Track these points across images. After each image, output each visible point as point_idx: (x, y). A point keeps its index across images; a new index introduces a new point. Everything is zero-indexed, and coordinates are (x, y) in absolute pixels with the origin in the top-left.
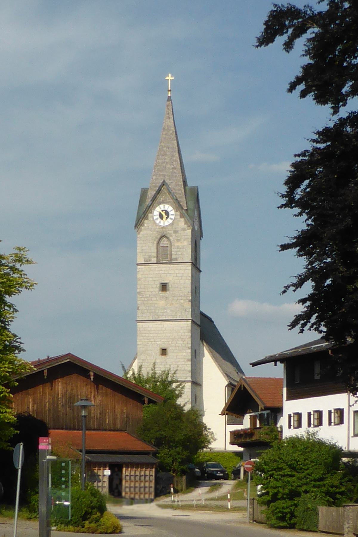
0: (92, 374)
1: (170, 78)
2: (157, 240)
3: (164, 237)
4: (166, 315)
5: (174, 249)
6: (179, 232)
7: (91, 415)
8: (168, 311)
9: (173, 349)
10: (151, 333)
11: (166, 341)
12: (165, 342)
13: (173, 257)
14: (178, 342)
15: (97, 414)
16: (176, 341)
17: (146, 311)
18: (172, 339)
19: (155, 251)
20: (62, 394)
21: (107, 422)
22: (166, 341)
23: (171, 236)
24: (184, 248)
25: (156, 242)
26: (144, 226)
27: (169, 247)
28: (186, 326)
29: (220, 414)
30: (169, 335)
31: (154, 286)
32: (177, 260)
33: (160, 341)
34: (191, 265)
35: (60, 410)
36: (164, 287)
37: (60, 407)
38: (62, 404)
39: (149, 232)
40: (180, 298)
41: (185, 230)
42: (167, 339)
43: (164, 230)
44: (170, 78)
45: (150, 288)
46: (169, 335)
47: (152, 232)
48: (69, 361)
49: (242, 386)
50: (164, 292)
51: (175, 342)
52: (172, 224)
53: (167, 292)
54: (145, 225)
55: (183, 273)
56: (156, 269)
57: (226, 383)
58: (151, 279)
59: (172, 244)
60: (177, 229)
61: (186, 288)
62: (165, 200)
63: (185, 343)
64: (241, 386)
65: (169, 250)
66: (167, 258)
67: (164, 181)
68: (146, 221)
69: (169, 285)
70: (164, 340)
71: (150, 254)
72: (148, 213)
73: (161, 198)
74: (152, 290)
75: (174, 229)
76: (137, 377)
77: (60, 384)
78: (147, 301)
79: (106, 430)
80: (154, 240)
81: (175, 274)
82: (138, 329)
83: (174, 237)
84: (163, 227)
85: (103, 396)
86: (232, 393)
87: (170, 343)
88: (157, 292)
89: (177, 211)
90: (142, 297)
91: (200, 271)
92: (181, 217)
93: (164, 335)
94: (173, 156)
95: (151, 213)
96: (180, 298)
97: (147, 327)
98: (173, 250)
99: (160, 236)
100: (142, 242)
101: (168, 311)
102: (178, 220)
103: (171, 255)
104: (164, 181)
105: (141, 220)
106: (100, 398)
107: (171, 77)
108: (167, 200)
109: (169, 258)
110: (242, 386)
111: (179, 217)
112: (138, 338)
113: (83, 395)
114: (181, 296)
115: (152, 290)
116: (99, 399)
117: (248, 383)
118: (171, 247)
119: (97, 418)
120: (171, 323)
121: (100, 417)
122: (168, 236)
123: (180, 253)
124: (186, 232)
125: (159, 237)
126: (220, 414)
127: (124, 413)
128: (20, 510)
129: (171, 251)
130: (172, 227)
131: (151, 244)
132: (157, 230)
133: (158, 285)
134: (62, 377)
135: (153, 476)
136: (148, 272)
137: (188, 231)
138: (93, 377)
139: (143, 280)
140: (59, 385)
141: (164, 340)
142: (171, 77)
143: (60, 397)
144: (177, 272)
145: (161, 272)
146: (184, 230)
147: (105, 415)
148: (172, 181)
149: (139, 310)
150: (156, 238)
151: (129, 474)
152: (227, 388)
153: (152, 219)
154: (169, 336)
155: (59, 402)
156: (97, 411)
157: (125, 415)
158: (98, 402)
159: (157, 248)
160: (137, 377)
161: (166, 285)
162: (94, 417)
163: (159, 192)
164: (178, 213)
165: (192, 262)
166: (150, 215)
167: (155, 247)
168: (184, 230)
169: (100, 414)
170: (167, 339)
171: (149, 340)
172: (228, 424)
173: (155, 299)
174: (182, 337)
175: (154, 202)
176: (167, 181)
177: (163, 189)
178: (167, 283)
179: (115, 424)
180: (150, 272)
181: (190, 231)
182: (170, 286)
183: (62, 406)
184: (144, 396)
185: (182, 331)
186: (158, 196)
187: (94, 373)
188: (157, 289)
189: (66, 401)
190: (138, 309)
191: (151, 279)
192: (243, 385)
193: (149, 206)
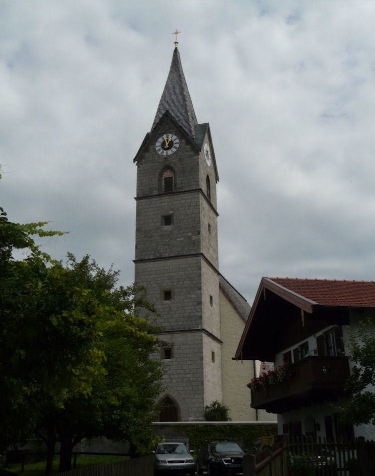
9: (179, 290)
13: (178, 186)
29: (233, 359)
32: (182, 189)
36: (168, 220)
64: (263, 292)
74: (153, 225)
76: (125, 280)
83: (179, 166)
84: (166, 158)
86: (271, 279)
91: (217, 215)
117: (221, 371)
120: (177, 260)
123: (186, 182)
126: (233, 359)
128: (231, 420)
135: (256, 422)
159: (160, 180)
160: (125, 280)
164: (184, 141)
166: (151, 147)
171: (148, 283)
174: (190, 276)
178: (171, 216)
180: (151, 206)
185: (190, 269)
191: (152, 213)
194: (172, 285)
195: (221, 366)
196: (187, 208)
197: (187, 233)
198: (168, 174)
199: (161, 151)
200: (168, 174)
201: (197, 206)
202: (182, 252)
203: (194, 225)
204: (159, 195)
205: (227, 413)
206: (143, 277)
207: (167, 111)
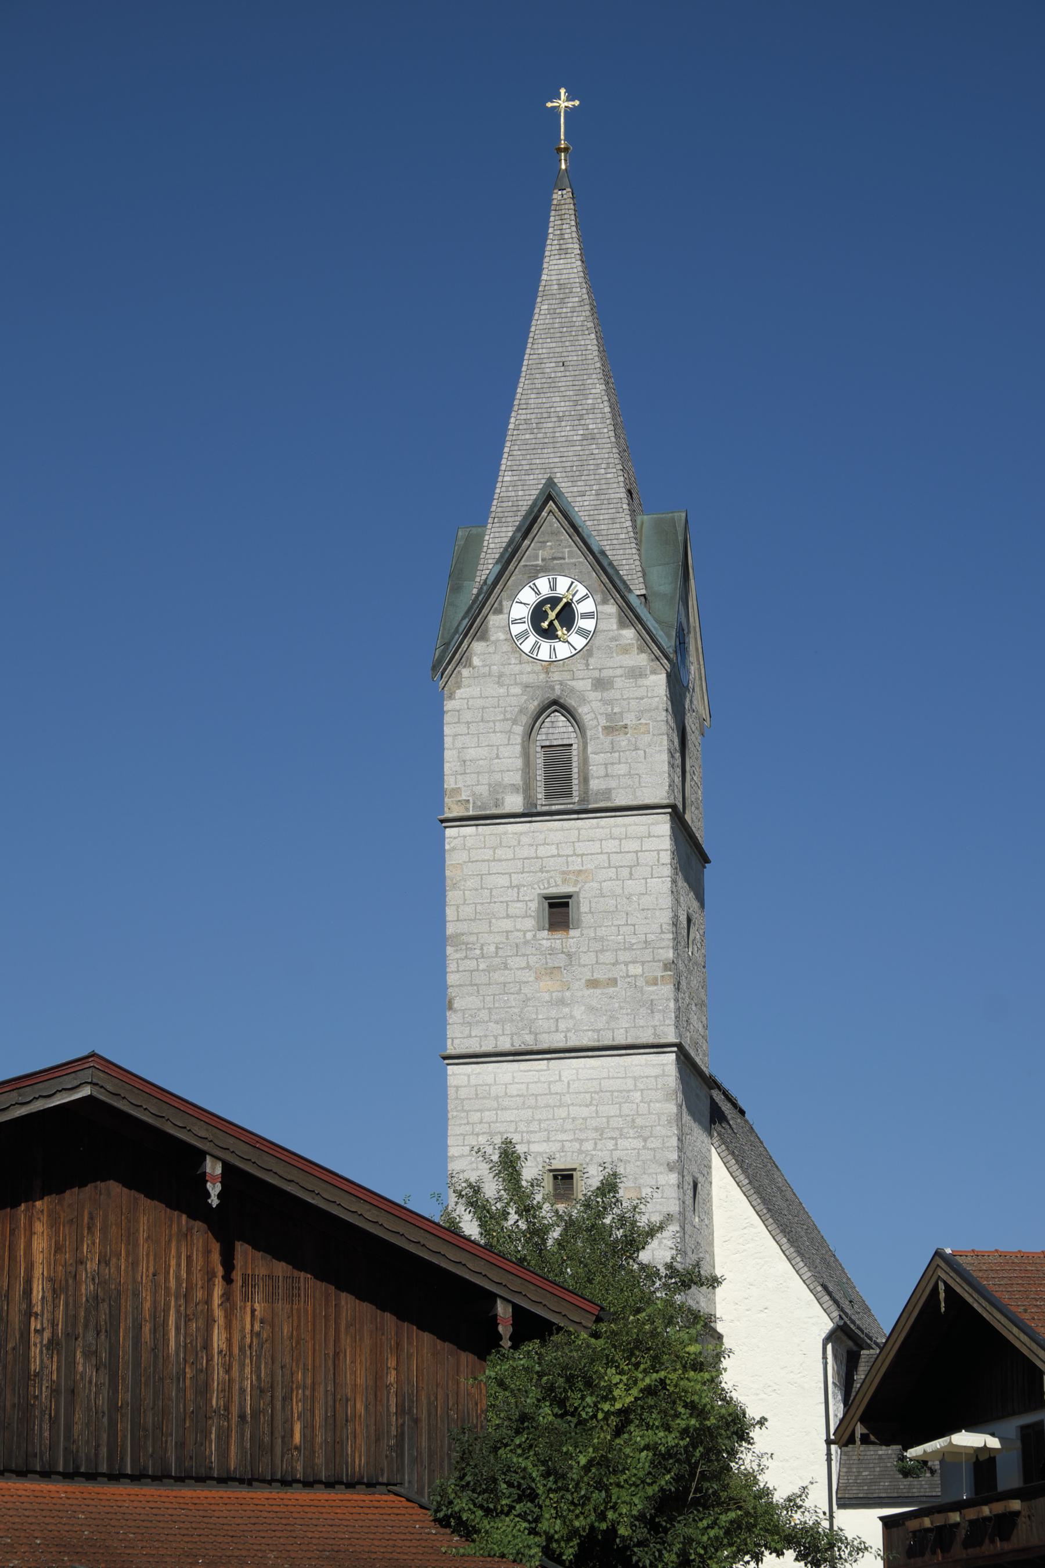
0: (213, 1168)
1: (563, 102)
2: (524, 719)
3: (554, 708)
4: (568, 1030)
5: (596, 753)
6: (619, 683)
7: (208, 1401)
8: (578, 1012)
10: (505, 1109)
11: (571, 1141)
12: (568, 1144)
13: (594, 784)
14: (622, 1143)
15: (242, 1391)
16: (612, 1138)
17: (483, 1015)
18: (596, 1129)
19: (519, 763)
20: (50, 1279)
21: (297, 1438)
22: (571, 1141)
23: (584, 700)
24: (637, 749)
25: (519, 729)
26: (469, 664)
27: (575, 747)
28: (657, 1071)
30: (585, 1112)
31: (517, 908)
33: (548, 1140)
34: (668, 817)
35: (35, 1366)
37: (35, 1351)
38: (47, 1335)
39: (493, 690)
40: (627, 953)
41: (642, 675)
42: (574, 1131)
43: (556, 677)
44: (563, 102)
45: (497, 919)
46: (585, 1112)
47: (502, 691)
48: (89, 1098)
49: (942, 1295)
50: (559, 935)
51: (610, 1145)
52: (586, 653)
53: (572, 933)
54: (476, 661)
55: (636, 852)
56: (525, 840)
57: (826, 1325)
58: (504, 881)
59: (589, 733)
60: (605, 673)
61: (649, 914)
62: (554, 559)
63: (649, 1145)
64: (935, 1290)
65: (575, 759)
66: (569, 795)
67: (550, 483)
68: (478, 647)
69: (578, 903)
70: (564, 1137)
71: (497, 777)
72: (485, 611)
73: (537, 552)
74: (507, 924)
75: (596, 674)
77: (39, 1227)
78: (435, 1534)
79: (286, 1483)
80: (515, 722)
81: (605, 857)
82: (451, 1092)
83: (596, 705)
85: (271, 1298)
87: (588, 1146)
88: (529, 936)
89: (605, 602)
90: (466, 957)
91: (706, 860)
92: (622, 625)
93: (562, 1113)
94: (582, 392)
95: (499, 611)
96: (624, 956)
97: (490, 1080)
98: (592, 758)
99: (536, 703)
100: (463, 729)
101: (578, 1012)
102: (611, 634)
103: (585, 780)
104: (550, 483)
105: (458, 638)
106: (257, 1306)
107: (568, 99)
108: (564, 559)
109: (575, 793)
110: (942, 1295)
111: (613, 624)
112: (453, 1130)
113: (167, 1289)
114: (630, 948)
115: (507, 924)
116: (253, 1311)
118: (585, 748)
119: (242, 1417)
121: (255, 1414)
122: (571, 702)
123: (622, 769)
124: (641, 682)
125: (533, 706)
127: (388, 1387)
129: (585, 762)
130: (587, 665)
131: (499, 738)
132: (525, 679)
133: (534, 906)
134: (55, 1186)
136: (488, 854)
137: (653, 678)
138: (218, 1187)
139: (469, 884)
140: (32, 1233)
141: (564, 1137)
142: (568, 99)
143: (37, 1294)
144: (611, 846)
145: (542, 851)
146: (635, 674)
147: (287, 1399)
148: (581, 486)
149: (456, 1011)
150: (521, 711)
151: (458, 776)
152: (829, 1347)
153: (501, 636)
154: (585, 1119)
155: (35, 1324)
156: (242, 1378)
157: (393, 1401)
158: (248, 1327)
159: (526, 755)
161: (567, 905)
162: (227, 1408)
163: (528, 527)
165: (671, 801)
166: (494, 620)
167: (518, 749)
168: (635, 674)
169: (259, 1391)
170: (574, 1131)
172: (842, 1506)
173: (524, 965)
174: (639, 1121)
175: (511, 567)
176: (564, 486)
177: (544, 514)
178: (570, 897)
179: (336, 1446)
180: (500, 853)
181: (663, 677)
182: (584, 908)
183: (53, 1344)
184: (492, 1297)
186: (526, 542)
187: (227, 1167)
188: (530, 923)
189: (71, 1319)
190: (450, 1008)
191: (504, 881)
192: (948, 1289)
193: (489, 582)
194: (580, 1152)
195: (674, 929)
196: (625, 872)
197: (626, 964)
198: (558, 730)
199: (524, 627)
200: (558, 730)
201: (710, 1151)
202: (610, 1035)
203: (650, 937)
204: (529, 814)
205: (751, 1478)
206: (475, 1117)
207: (899, 1471)
